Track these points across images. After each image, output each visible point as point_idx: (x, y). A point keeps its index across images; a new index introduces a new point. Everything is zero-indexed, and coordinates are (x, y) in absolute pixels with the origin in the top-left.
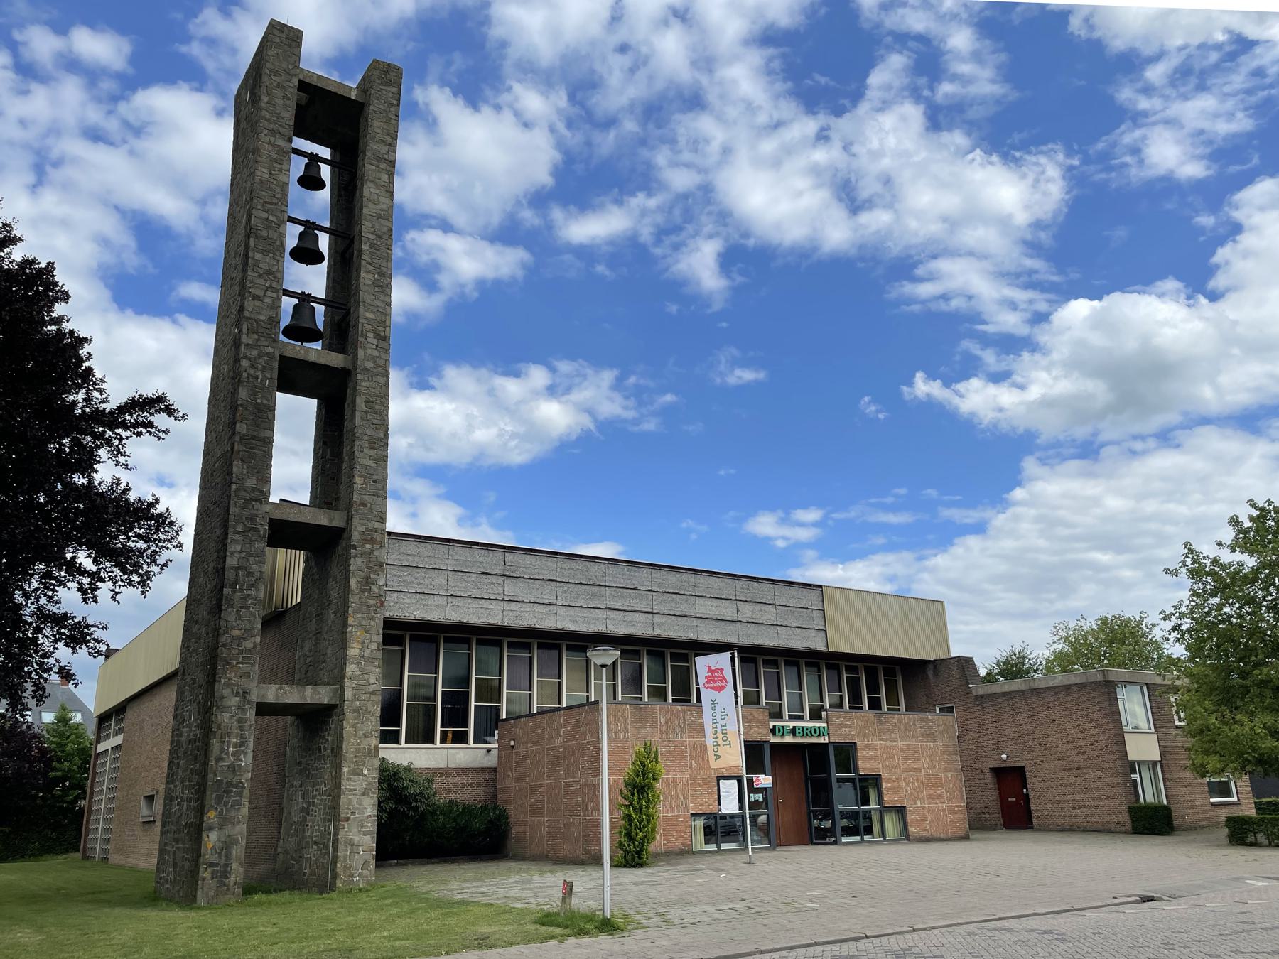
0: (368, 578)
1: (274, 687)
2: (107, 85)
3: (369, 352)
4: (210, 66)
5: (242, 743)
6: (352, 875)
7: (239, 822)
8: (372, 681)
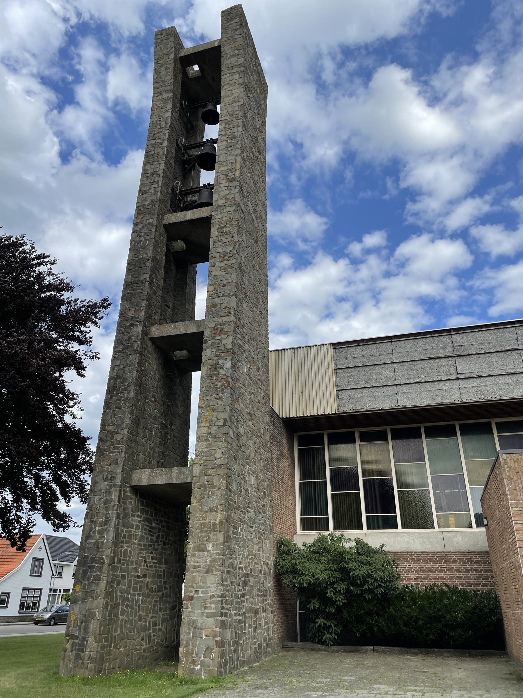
0: (216, 364)
1: (147, 471)
2: (384, 252)
3: (222, 193)
4: (421, 223)
5: (106, 523)
6: (194, 663)
7: (97, 596)
8: (218, 455)
